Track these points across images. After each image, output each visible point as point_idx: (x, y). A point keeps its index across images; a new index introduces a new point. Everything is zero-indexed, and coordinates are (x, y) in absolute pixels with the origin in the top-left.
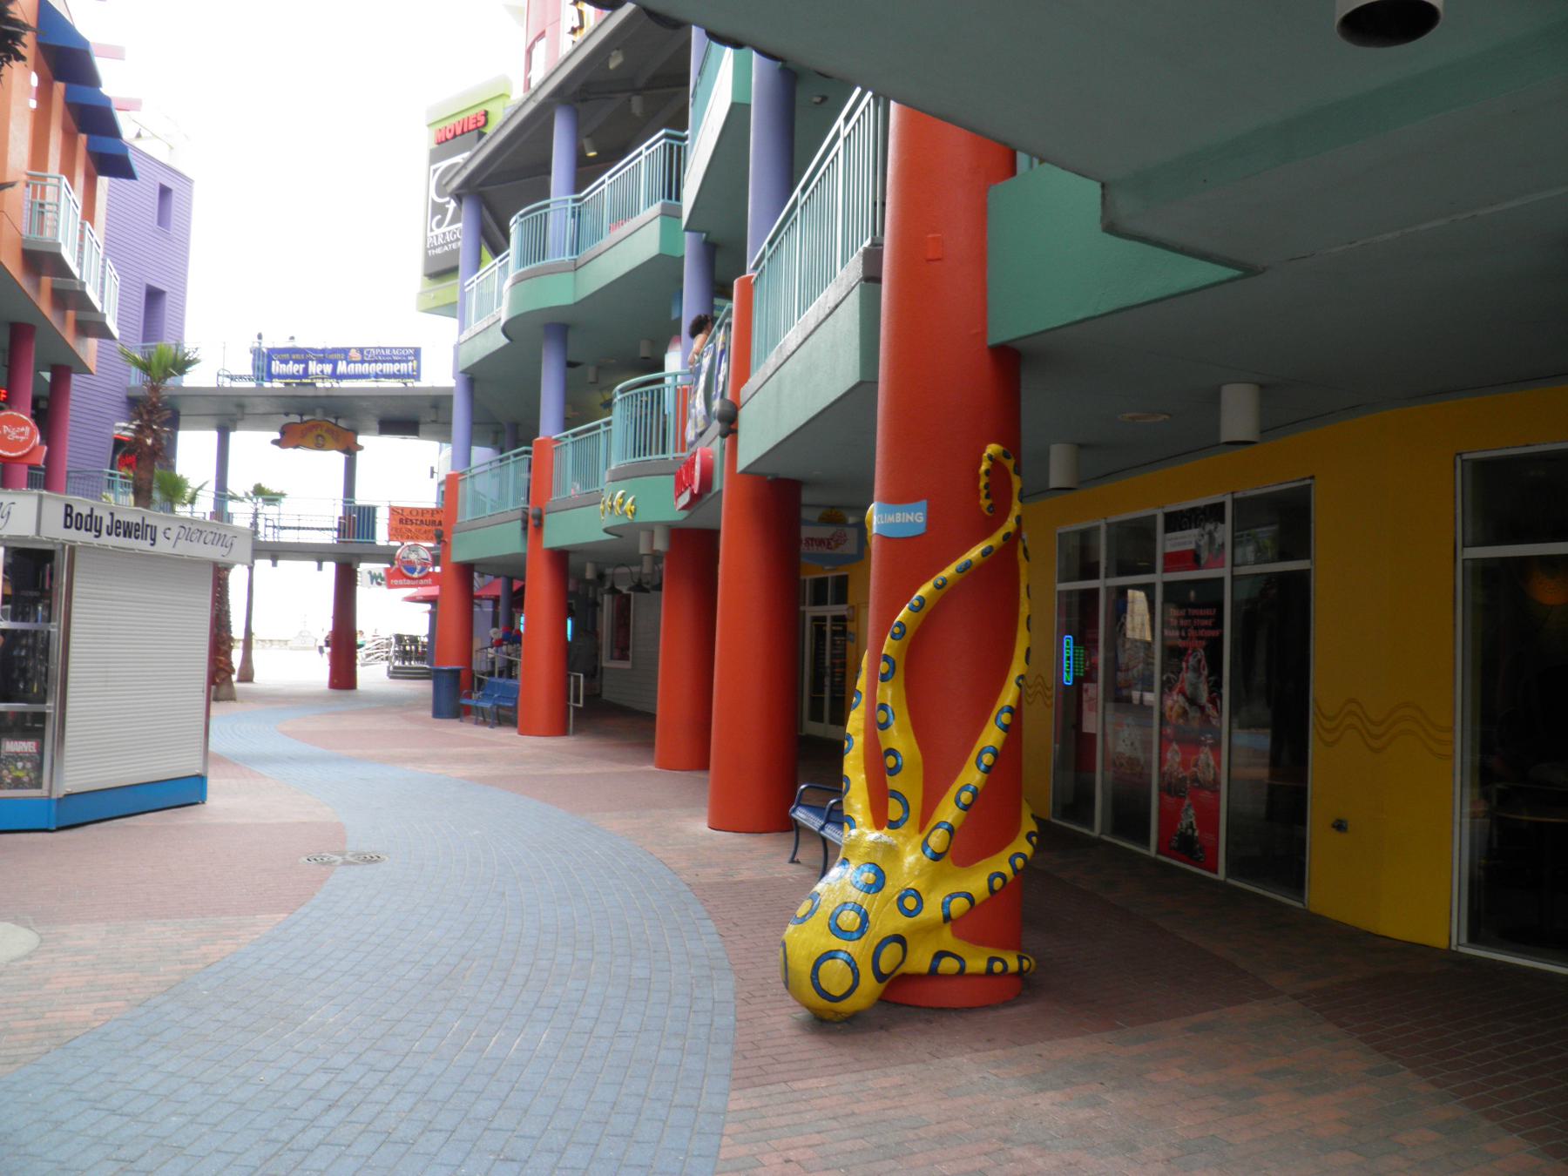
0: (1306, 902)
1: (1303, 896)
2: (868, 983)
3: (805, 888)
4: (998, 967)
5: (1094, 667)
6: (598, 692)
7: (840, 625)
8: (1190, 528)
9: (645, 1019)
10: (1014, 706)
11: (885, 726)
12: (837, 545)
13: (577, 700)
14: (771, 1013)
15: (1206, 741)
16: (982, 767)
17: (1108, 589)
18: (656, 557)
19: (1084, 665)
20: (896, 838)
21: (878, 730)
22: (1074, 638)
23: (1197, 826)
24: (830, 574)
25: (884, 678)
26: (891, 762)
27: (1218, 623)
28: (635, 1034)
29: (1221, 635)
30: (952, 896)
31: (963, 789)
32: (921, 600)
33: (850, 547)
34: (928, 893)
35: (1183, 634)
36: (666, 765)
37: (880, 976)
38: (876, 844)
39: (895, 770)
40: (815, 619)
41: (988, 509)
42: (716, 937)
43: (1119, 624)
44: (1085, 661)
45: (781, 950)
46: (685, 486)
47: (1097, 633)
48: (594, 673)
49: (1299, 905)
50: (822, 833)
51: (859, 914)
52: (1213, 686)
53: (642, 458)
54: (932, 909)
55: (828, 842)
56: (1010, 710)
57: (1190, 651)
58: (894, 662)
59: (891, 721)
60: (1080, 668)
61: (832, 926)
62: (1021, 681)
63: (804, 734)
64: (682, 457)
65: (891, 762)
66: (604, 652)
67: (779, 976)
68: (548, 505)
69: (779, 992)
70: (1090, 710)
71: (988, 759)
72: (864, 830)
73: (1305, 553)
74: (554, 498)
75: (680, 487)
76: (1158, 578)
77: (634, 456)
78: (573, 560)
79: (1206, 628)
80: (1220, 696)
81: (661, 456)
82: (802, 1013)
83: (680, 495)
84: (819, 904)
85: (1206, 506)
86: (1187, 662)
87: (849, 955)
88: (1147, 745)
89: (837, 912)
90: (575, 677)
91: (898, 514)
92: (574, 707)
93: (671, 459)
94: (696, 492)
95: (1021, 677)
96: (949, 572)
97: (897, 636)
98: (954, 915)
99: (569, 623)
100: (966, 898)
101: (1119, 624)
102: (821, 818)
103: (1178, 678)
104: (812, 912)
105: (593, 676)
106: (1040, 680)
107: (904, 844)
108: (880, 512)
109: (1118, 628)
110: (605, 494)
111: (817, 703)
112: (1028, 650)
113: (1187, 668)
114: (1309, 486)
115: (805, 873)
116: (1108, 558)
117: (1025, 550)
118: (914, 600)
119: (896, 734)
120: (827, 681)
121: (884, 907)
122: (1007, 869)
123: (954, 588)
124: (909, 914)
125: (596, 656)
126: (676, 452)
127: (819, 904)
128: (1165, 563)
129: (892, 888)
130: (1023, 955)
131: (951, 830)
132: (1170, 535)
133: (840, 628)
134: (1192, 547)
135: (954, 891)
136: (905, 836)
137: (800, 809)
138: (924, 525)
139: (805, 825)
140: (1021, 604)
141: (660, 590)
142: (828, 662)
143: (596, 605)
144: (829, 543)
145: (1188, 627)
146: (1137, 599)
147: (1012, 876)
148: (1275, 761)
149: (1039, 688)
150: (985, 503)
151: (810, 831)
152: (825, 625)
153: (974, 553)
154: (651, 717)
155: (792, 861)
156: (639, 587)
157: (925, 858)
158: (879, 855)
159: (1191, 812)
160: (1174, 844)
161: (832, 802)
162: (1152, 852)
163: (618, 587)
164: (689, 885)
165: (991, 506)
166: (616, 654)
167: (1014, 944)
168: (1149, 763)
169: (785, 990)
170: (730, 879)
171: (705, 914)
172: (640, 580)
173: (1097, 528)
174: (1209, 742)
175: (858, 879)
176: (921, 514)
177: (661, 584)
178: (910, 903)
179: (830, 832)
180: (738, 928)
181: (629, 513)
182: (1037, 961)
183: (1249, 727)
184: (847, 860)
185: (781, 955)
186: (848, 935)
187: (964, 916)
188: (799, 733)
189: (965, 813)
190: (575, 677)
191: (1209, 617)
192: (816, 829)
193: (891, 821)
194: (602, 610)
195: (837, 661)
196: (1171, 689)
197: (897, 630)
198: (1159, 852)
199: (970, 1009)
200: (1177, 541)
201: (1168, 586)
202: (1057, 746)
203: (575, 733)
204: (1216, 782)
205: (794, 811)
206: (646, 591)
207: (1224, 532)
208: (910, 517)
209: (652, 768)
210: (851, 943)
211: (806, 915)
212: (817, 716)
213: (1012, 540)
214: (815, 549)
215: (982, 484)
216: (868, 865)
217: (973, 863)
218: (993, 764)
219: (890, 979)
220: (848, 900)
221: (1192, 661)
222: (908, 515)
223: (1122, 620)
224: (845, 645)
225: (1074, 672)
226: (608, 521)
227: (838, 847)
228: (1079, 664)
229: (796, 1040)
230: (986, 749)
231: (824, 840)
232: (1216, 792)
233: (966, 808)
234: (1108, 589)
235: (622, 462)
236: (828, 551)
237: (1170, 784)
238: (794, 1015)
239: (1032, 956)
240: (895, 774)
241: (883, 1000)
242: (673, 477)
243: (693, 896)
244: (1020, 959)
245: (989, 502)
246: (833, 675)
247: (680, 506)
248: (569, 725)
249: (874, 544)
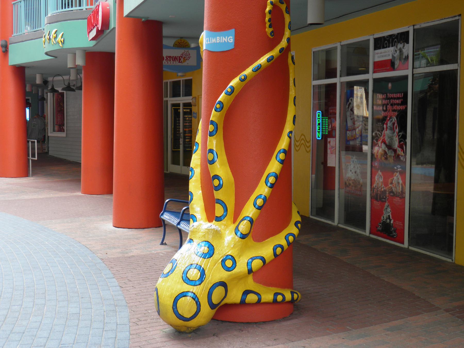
0: (454, 259)
1: (452, 255)
2: (206, 310)
3: (168, 258)
4: (280, 298)
5: (334, 129)
6: (46, 151)
7: (187, 109)
8: (389, 47)
9: (77, 336)
10: (287, 149)
11: (212, 162)
12: (185, 60)
13: (33, 155)
14: (150, 330)
15: (397, 169)
16: (269, 184)
17: (341, 83)
18: (78, 70)
19: (328, 128)
20: (220, 226)
21: (208, 164)
22: (322, 112)
23: (392, 218)
24: (181, 78)
25: (211, 134)
26: (216, 182)
27: (405, 102)
28: (71, 345)
29: (406, 108)
30: (253, 259)
31: (257, 198)
32: (233, 88)
33: (192, 62)
34: (239, 257)
35: (385, 109)
36: (88, 192)
37: (212, 306)
38: (209, 231)
39: (219, 188)
40: (173, 105)
41: (271, 34)
42: (118, 288)
43: (348, 104)
44: (328, 125)
45: (155, 293)
46: (93, 26)
47: (336, 109)
48: (43, 140)
49: (450, 260)
50: (178, 226)
51: (199, 271)
52: (401, 138)
53: (67, 9)
54: (242, 267)
55: (182, 232)
56: (285, 151)
57: (388, 118)
58: (217, 125)
59: (216, 159)
60: (325, 130)
61: (184, 278)
62: (290, 135)
63: (168, 172)
64: (91, 9)
65: (216, 182)
66: (49, 127)
67: (155, 309)
68: (11, 39)
69: (155, 317)
70: (332, 153)
71: (272, 180)
72: (202, 222)
73: (455, 60)
74: (14, 34)
75: (90, 26)
76: (370, 76)
77: (62, 8)
78: (27, 72)
79: (398, 104)
80: (406, 144)
81: (78, 8)
82: (169, 329)
83: (90, 31)
84: (176, 266)
85: (398, 34)
86: (387, 124)
87: (194, 294)
88: (364, 174)
89: (187, 269)
90: (32, 142)
91: (217, 38)
92: (32, 160)
93: (84, 10)
94: (100, 29)
95: (291, 132)
96: (248, 71)
97: (218, 110)
98: (254, 270)
99: (28, 111)
100: (260, 259)
101: (348, 104)
102: (178, 218)
103: (382, 134)
104: (172, 270)
105: (44, 140)
106: (303, 137)
107: (225, 230)
108: (207, 37)
109: (347, 106)
110: (45, 31)
111: (175, 153)
112: (295, 117)
113: (387, 128)
114: (457, 21)
115: (170, 250)
116: (341, 66)
117: (292, 58)
118: (228, 89)
119: (219, 167)
120: (181, 141)
121: (214, 266)
122: (284, 243)
123: (251, 81)
124: (228, 269)
125: (44, 130)
126: (88, 5)
127: (176, 266)
128: (374, 67)
129: (218, 255)
130: (293, 291)
131: (251, 221)
132: (377, 51)
133: (189, 110)
134: (390, 57)
135: (254, 255)
136: (225, 225)
137: (165, 213)
138: (234, 44)
139: (170, 223)
140: (290, 90)
141: (81, 89)
142: (181, 131)
143: (43, 99)
144: (180, 59)
145: (387, 104)
146: (359, 91)
147: (287, 246)
148: (437, 180)
149: (303, 142)
150: (269, 30)
151: (172, 226)
152: (179, 109)
153: (263, 60)
154: (78, 164)
155: (162, 243)
156: (69, 88)
157: (236, 237)
158: (211, 237)
159: (389, 210)
160: (379, 228)
161: (184, 208)
162: (367, 233)
163: (56, 89)
164: (102, 259)
165: (272, 32)
166: (56, 128)
167: (289, 285)
168: (366, 184)
169: (158, 316)
170: (126, 255)
171: (112, 276)
172: (69, 83)
173: (336, 48)
174: (399, 170)
175: (199, 251)
176: (232, 37)
177: (81, 86)
178: (229, 263)
179: (183, 226)
180: (131, 283)
181: (60, 43)
182: (302, 295)
183: (422, 164)
184: (192, 240)
185: (155, 296)
186: (194, 282)
187: (260, 270)
188: (165, 172)
189: (259, 211)
190: (32, 142)
191: (398, 98)
192: (175, 225)
193: (217, 217)
194: (47, 102)
195: (187, 130)
196: (377, 140)
197: (218, 106)
198: (371, 233)
199: (265, 322)
200: (382, 55)
201: (376, 81)
202: (314, 176)
203: (33, 175)
204: (403, 192)
205: (162, 214)
206: (73, 90)
207: (408, 49)
208: (225, 39)
209: (80, 194)
210: (195, 287)
211: (169, 272)
212: (176, 162)
213: (285, 52)
214: (172, 63)
215: (267, 19)
216: (204, 243)
217: (265, 240)
218: (275, 183)
219: (218, 307)
220: (193, 263)
221: (389, 124)
222: (224, 38)
223: (350, 101)
224: (191, 120)
225: (322, 132)
226: (48, 48)
227: (187, 234)
228: (325, 127)
229: (165, 344)
230: (271, 174)
231: (180, 231)
232: (404, 198)
233: (260, 208)
234: (341, 83)
235: (54, 12)
236: (180, 64)
237: (377, 194)
238: (164, 330)
239: (299, 292)
240: (219, 190)
241: (214, 319)
242: (86, 20)
243: (105, 265)
244: (292, 293)
245: (271, 30)
246: (185, 138)
247: (91, 38)
248: (29, 167)
249: (204, 56)
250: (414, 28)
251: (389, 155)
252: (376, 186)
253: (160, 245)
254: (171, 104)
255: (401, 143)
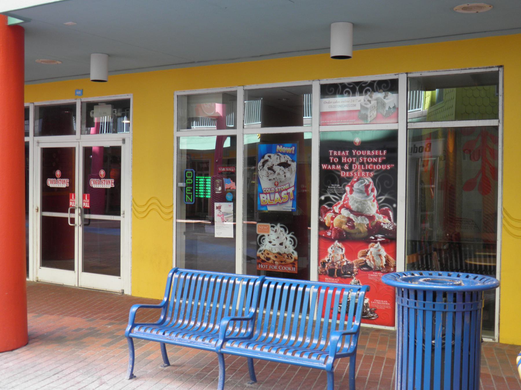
250: (407, 76)
251: (359, 222)
252: (329, 260)
253: (129, 379)
254: (41, 148)
255: (384, 209)
